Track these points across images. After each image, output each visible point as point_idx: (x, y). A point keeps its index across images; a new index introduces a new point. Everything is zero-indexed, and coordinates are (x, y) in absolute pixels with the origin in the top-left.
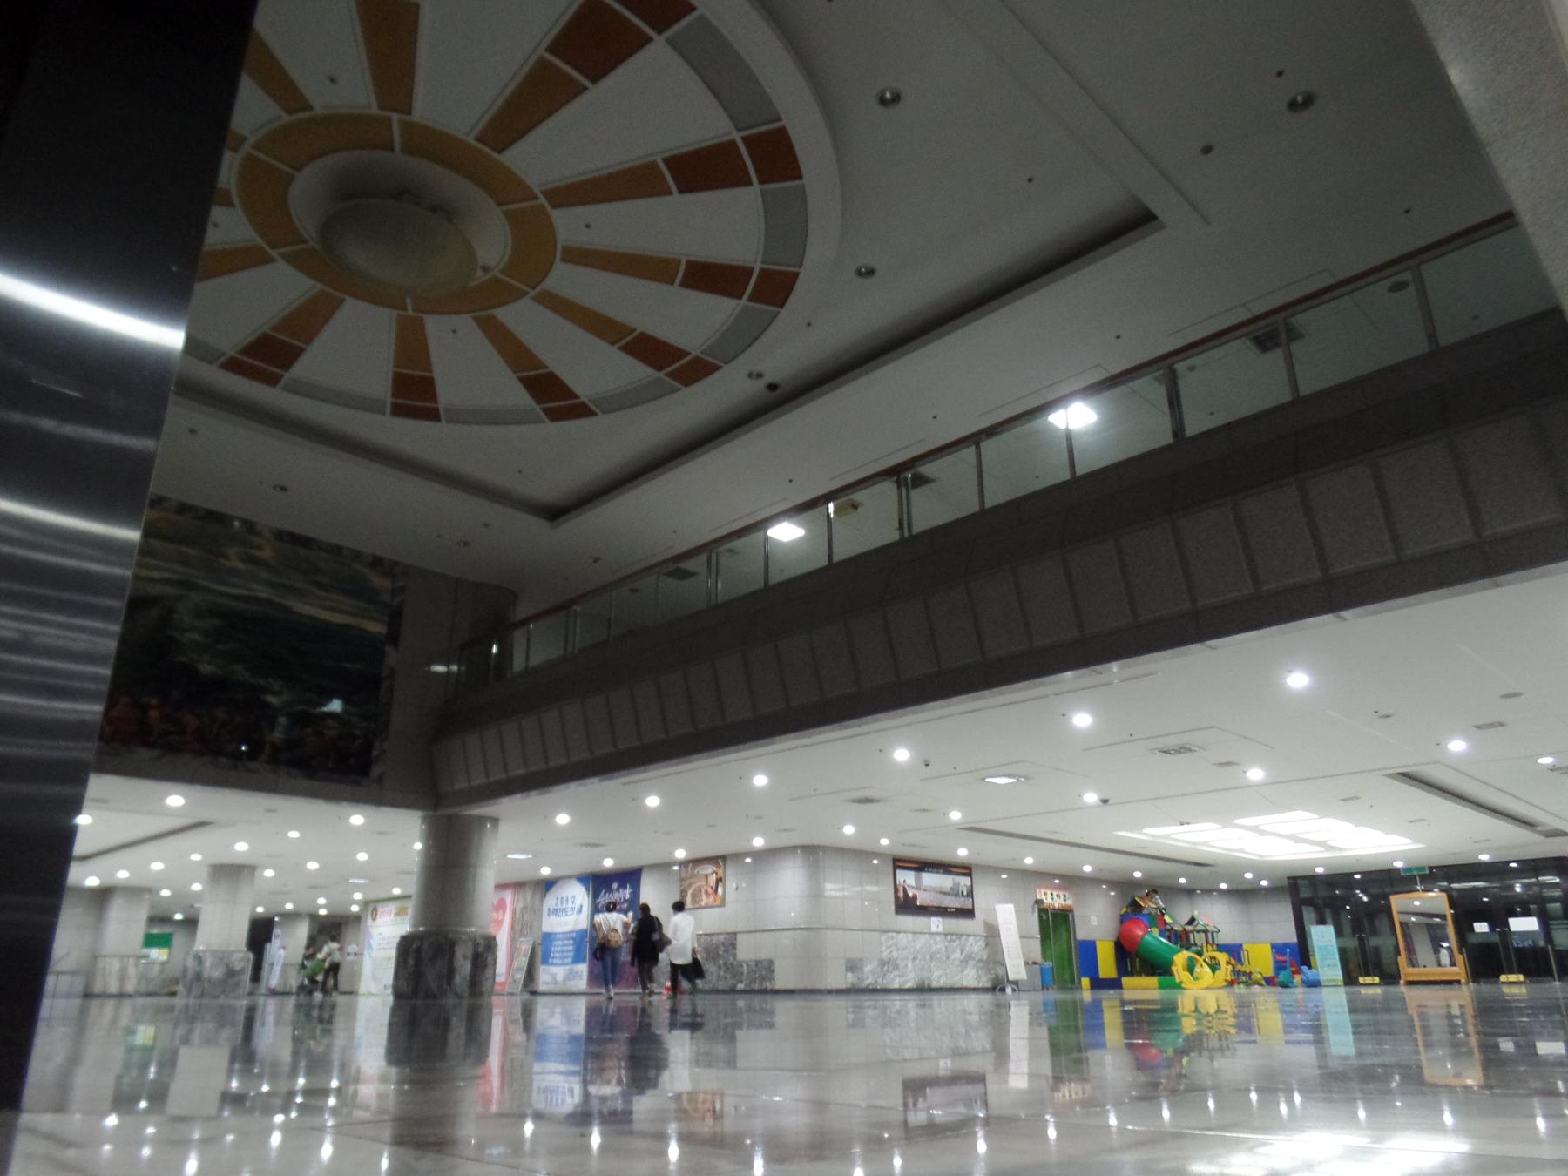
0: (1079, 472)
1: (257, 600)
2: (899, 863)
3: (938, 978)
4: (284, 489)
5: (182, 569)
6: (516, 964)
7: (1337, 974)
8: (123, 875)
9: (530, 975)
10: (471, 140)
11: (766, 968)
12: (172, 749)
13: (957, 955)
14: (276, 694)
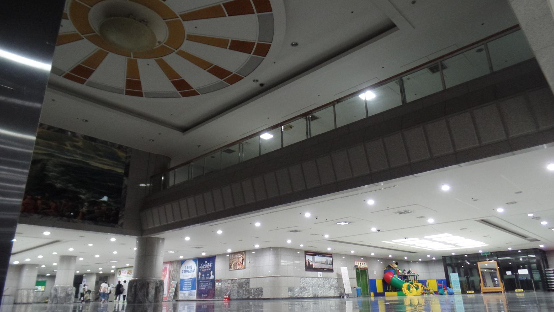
2: (307, 253)
4: (86, 121)
5: (51, 150)
6: (170, 291)
7: (459, 290)
8: (28, 260)
9: (176, 294)
12: (46, 214)
14: (84, 194)
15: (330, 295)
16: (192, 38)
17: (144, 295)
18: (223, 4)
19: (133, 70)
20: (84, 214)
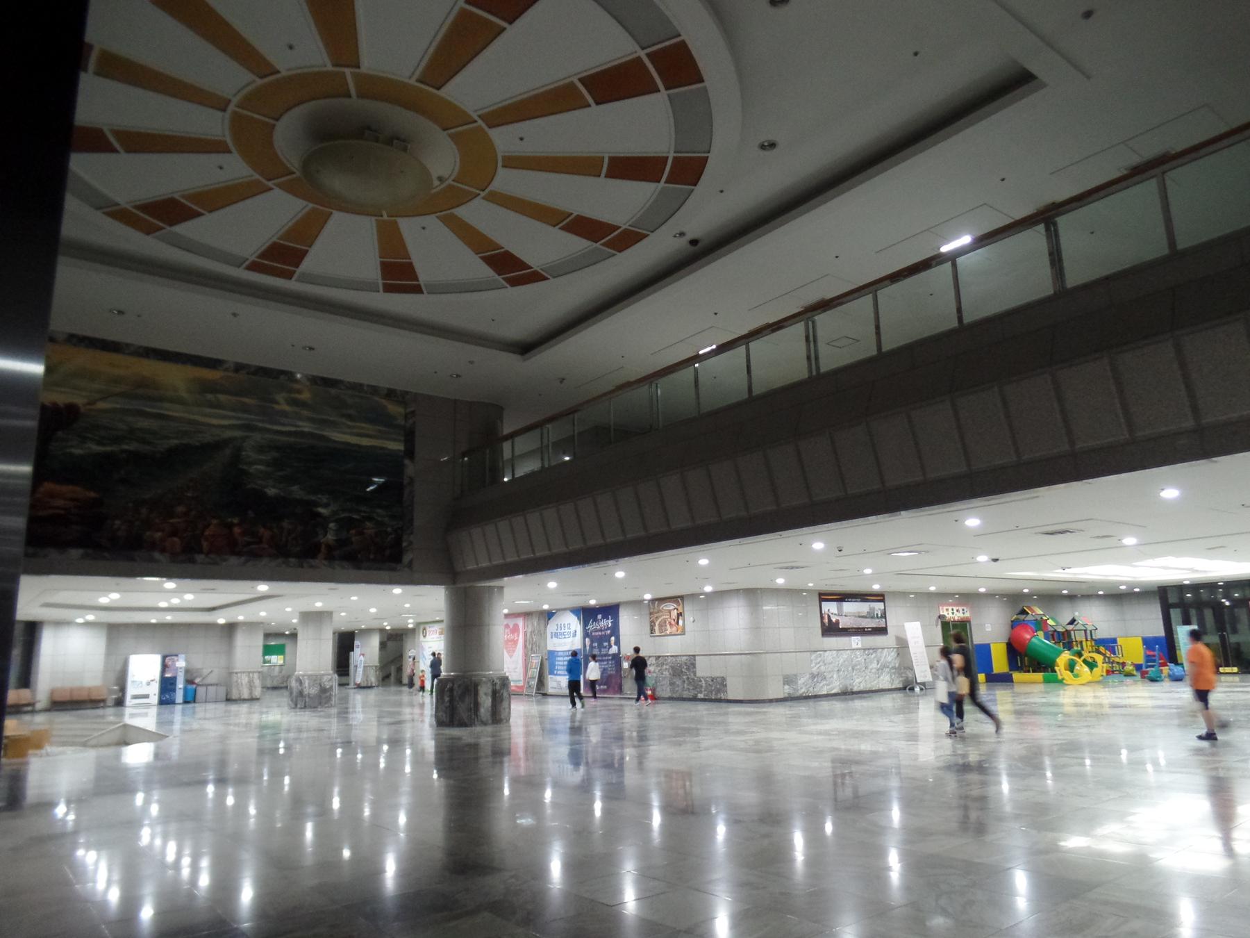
0: (967, 319)
1: (302, 434)
2: (824, 597)
3: (858, 684)
4: (311, 349)
5: (246, 416)
6: (530, 673)
8: (241, 618)
9: (541, 682)
10: (413, 82)
11: (720, 684)
13: (874, 665)
14: (326, 506)
16: (513, 162)
18: (580, 80)
19: (391, 241)
20: (330, 548)
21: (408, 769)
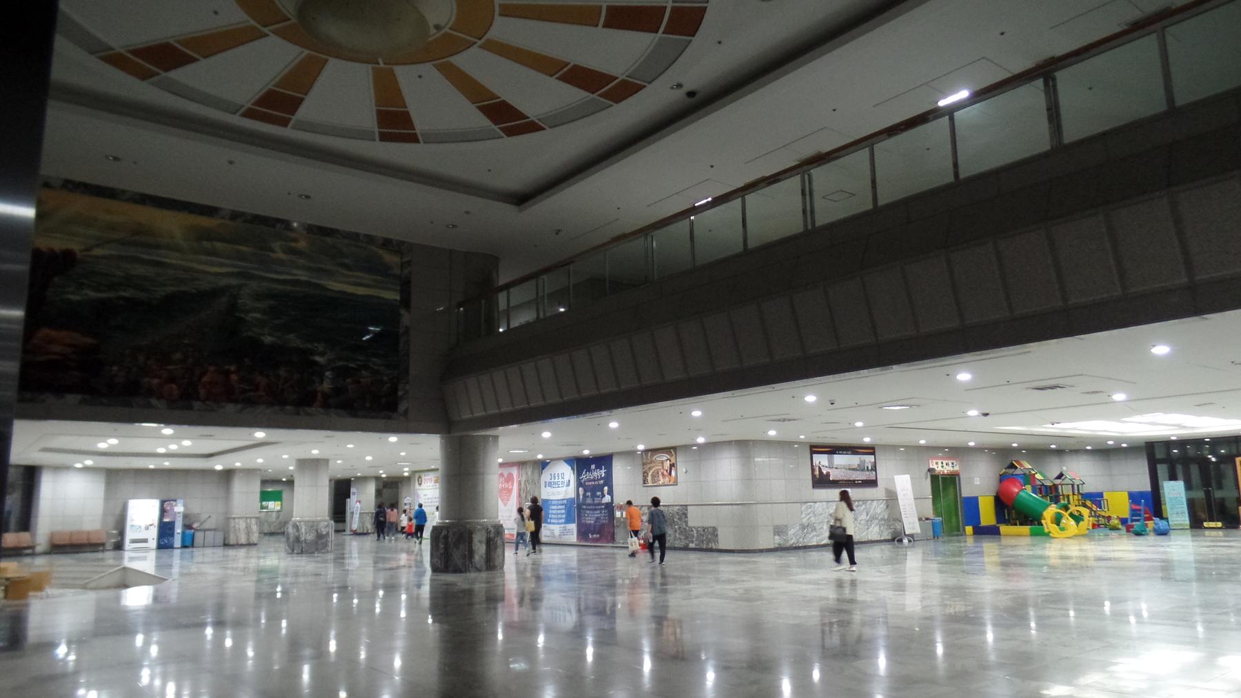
1: (297, 283)
2: (815, 449)
4: (307, 197)
7: (1185, 520)
8: (238, 464)
12: (250, 402)
14: (322, 354)
15: (870, 538)
17: (464, 557)
19: (387, 90)
20: (326, 397)
21: (403, 614)
